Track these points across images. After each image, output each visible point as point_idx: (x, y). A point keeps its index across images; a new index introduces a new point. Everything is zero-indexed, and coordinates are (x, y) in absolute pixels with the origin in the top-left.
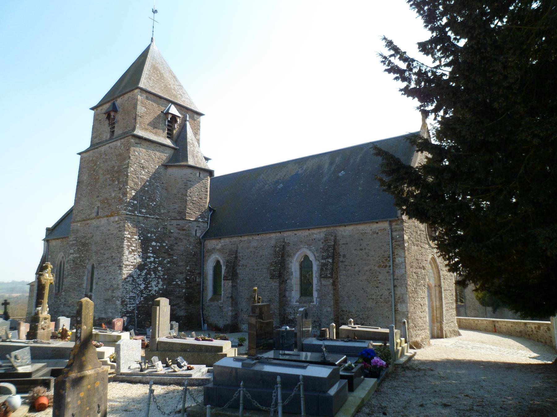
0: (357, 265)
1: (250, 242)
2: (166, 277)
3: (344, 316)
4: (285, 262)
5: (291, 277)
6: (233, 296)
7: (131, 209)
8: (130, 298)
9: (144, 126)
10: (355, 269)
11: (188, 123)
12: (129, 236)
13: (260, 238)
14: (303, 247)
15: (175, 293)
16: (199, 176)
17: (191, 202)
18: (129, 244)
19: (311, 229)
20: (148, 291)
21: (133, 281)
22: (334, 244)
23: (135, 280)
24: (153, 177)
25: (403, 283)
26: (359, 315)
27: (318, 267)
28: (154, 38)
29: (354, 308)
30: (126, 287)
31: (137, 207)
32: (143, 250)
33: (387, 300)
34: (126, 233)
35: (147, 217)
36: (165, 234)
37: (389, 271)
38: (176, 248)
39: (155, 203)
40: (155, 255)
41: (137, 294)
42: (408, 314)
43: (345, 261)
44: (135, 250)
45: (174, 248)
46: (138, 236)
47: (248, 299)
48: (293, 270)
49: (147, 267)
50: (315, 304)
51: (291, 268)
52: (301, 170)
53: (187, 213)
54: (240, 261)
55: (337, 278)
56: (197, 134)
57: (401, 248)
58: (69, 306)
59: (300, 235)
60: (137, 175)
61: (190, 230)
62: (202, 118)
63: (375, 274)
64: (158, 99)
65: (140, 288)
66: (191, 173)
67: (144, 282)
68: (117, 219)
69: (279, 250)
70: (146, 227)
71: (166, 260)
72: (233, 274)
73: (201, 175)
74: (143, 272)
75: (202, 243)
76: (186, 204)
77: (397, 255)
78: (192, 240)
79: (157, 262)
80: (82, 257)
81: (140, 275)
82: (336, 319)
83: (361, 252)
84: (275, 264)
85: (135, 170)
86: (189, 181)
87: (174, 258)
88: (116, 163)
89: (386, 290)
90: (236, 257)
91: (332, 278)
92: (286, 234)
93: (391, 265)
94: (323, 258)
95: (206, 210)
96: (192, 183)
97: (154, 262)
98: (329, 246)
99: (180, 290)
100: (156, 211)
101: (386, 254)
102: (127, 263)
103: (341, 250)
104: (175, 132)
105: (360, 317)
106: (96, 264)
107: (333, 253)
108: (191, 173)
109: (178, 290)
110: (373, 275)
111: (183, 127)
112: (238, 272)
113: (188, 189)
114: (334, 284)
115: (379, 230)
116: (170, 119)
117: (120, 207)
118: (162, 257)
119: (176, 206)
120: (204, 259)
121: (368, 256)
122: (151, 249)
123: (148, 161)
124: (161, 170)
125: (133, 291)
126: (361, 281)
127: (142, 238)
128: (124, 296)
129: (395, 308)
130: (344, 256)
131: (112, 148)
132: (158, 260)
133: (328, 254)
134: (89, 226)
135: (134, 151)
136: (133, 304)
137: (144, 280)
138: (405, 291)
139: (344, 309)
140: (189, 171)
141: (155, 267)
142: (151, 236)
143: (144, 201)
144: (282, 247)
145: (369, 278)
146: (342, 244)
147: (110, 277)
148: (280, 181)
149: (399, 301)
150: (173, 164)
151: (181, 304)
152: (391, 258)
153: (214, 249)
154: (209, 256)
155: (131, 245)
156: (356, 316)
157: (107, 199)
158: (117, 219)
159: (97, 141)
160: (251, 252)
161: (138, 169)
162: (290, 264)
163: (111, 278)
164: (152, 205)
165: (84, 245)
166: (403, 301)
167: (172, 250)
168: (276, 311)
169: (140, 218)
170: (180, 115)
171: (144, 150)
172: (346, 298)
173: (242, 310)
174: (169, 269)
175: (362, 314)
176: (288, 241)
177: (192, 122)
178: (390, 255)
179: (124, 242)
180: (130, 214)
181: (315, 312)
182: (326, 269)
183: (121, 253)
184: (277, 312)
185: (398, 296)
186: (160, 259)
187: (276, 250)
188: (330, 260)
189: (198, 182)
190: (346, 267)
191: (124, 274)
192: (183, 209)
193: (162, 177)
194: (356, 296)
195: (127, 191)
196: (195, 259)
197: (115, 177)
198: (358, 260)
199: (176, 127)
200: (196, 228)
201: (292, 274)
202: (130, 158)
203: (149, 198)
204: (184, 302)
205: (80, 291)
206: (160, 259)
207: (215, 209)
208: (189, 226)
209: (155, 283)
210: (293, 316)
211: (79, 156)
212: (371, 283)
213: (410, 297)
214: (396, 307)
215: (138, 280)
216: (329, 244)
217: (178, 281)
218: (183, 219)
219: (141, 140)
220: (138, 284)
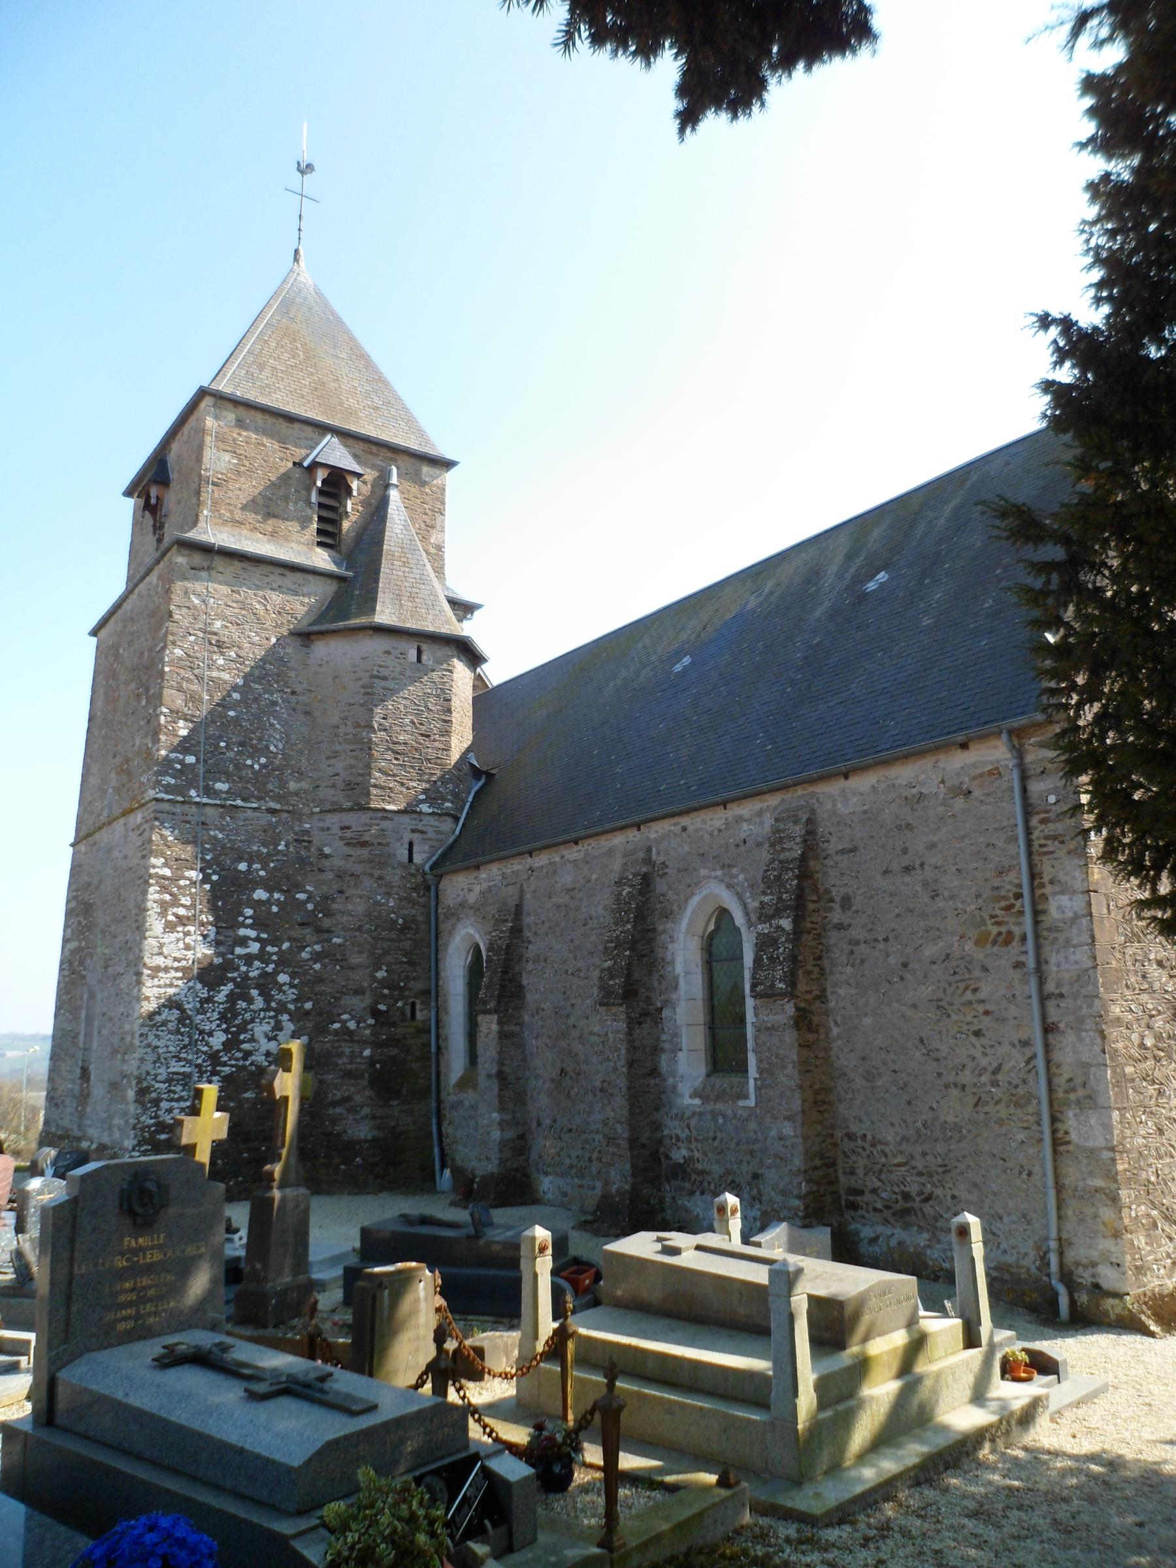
0: (896, 937)
2: (308, 1005)
3: (854, 1158)
4: (651, 940)
5: (674, 996)
6: (507, 1069)
7: (173, 781)
8: (169, 1081)
9: (231, 512)
10: (888, 955)
11: (394, 494)
12: (167, 872)
13: (582, 854)
14: (709, 877)
15: (340, 1062)
16: (419, 660)
17: (389, 749)
18: (167, 897)
20: (239, 1055)
21: (181, 1021)
22: (803, 855)
23: (189, 1017)
24: (257, 673)
25: (1084, 1011)
26: (912, 1157)
28: (301, 251)
29: (892, 1124)
30: (155, 1043)
31: (197, 776)
32: (217, 918)
33: (1021, 1091)
34: (153, 860)
35: (236, 807)
36: (302, 861)
37: (1022, 958)
39: (263, 760)
40: (263, 932)
41: (198, 1066)
42: (1113, 1160)
43: (849, 926)
44: (188, 918)
45: (335, 906)
46: (202, 870)
47: (553, 1080)
48: (679, 969)
49: (235, 975)
51: (673, 963)
53: (375, 786)
54: (530, 942)
55: (822, 997)
56: (433, 527)
57: (1069, 853)
59: (697, 830)
60: (196, 671)
61: (388, 844)
62: (450, 478)
63: (967, 976)
64: (282, 425)
65: (207, 1044)
66: (388, 653)
67: (224, 1026)
69: (629, 893)
70: (230, 840)
71: (308, 949)
73: (424, 657)
74: (219, 992)
75: (433, 888)
76: (371, 756)
77: (1051, 882)
78: (394, 876)
79: (275, 958)
81: (209, 1000)
82: (820, 1173)
83: (908, 879)
84: (615, 948)
85: (189, 656)
86: (378, 677)
87: (335, 940)
89: (1014, 1045)
90: (517, 931)
91: (792, 996)
92: (655, 831)
95: (446, 773)
96: (390, 684)
97: (262, 956)
98: (784, 865)
99: (352, 1052)
100: (270, 786)
101: (1007, 884)
102: (160, 961)
104: (346, 525)
105: (913, 1163)
107: (800, 896)
108: (388, 653)
109: (347, 1051)
110: (957, 977)
111: (377, 508)
112: (525, 982)
113: (376, 706)
115: (975, 778)
116: (324, 482)
118: (289, 939)
119: (339, 765)
120: (440, 942)
121: (935, 896)
122: (249, 912)
123: (238, 624)
124: (289, 650)
125: (183, 1055)
126: (915, 1006)
127: (215, 878)
128: (148, 1073)
129: (1054, 1132)
130: (846, 903)
132: (276, 949)
133: (780, 899)
135: (186, 593)
136: (180, 1099)
137: (223, 1018)
138: (1097, 1048)
139: (854, 1128)
140: (375, 646)
141: (264, 974)
142: (249, 871)
143: (224, 754)
144: (638, 880)
146: (837, 853)
148: (686, 646)
149: (1072, 1096)
150: (334, 626)
151: (358, 1099)
153: (461, 905)
154: (450, 933)
155: (175, 903)
156: (899, 1159)
161: (201, 653)
162: (670, 946)
164: (252, 766)
166: (1090, 1097)
167: (328, 914)
169: (209, 811)
170: (357, 468)
171: (225, 590)
172: (859, 1082)
173: (539, 1124)
175: (924, 1154)
176: (661, 859)
177: (414, 490)
178: (1020, 886)
179: (147, 892)
180: (169, 801)
181: (754, 1137)
182: (771, 959)
183: (140, 928)
185: (1066, 1076)
186: (286, 946)
187: (620, 894)
188: (786, 923)
189: (414, 680)
191: (147, 998)
192: (361, 775)
193: (292, 674)
194: (895, 1072)
195: (159, 724)
196: (407, 945)
198: (898, 916)
199: (349, 509)
200: (407, 837)
201: (676, 987)
202: (171, 616)
203: (241, 744)
204: (368, 1093)
206: (286, 946)
207: (493, 772)
208: (383, 830)
209: (266, 1028)
210: (684, 1152)
212: (954, 1017)
213: (1122, 1080)
214: (1059, 1125)
216: (786, 855)
218: (363, 808)
220: (202, 1032)
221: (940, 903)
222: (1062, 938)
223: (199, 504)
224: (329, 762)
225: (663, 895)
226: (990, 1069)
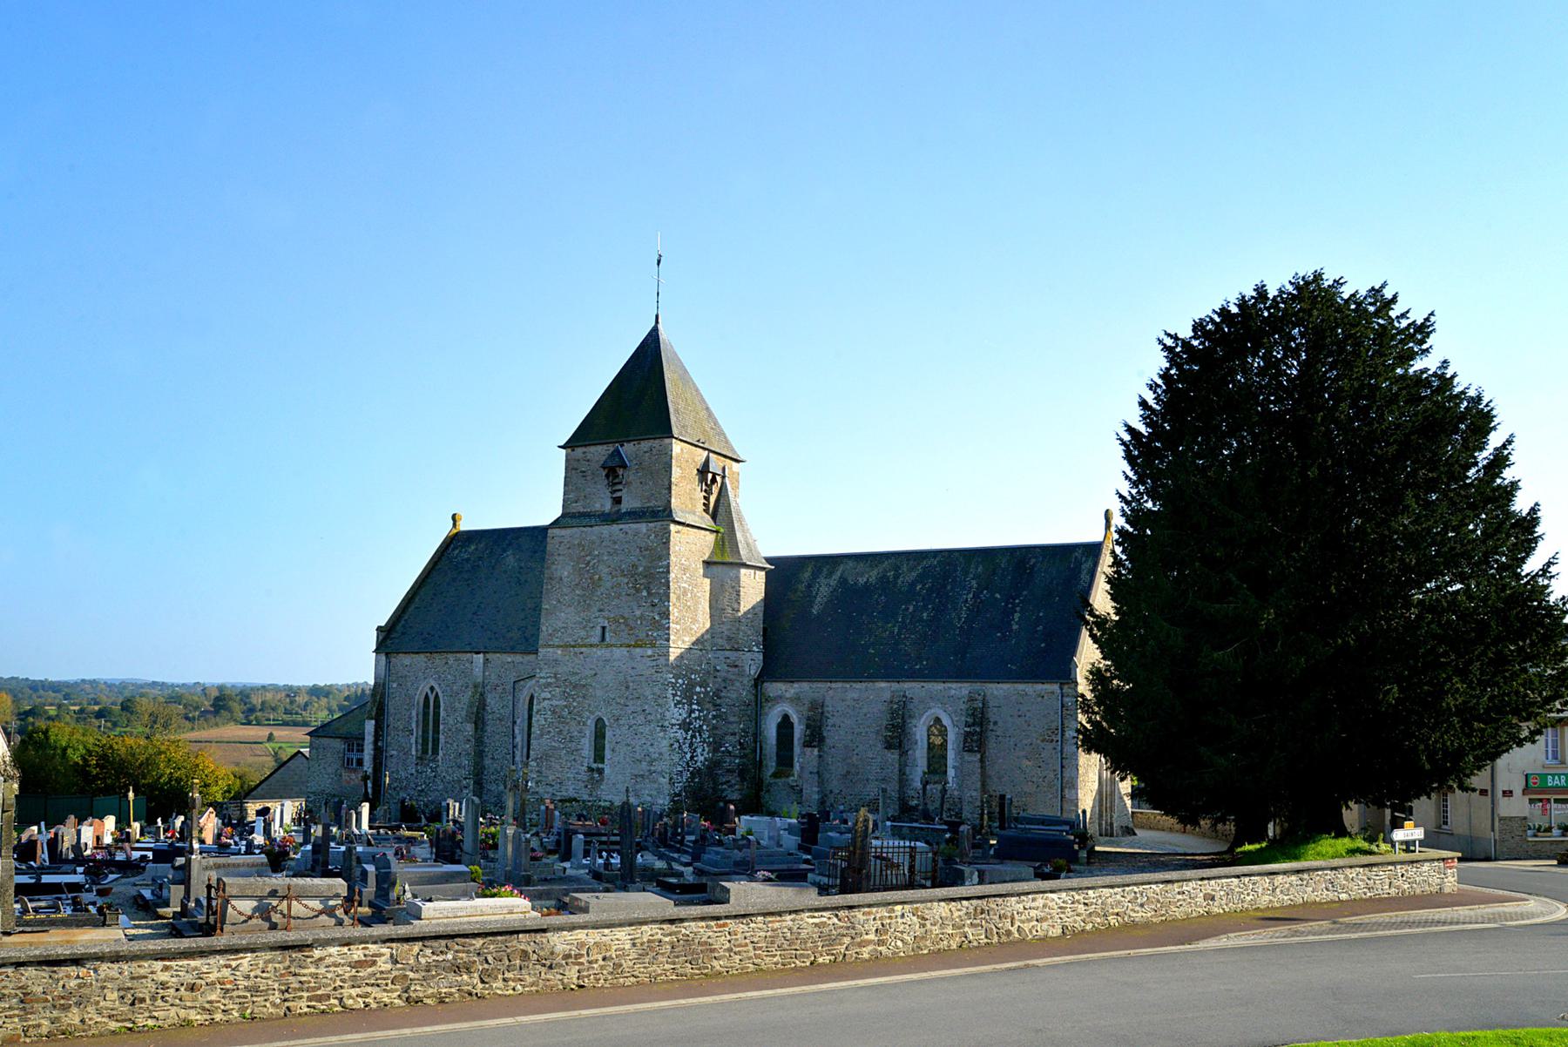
1: (846, 691)
5: (915, 747)
45: (723, 694)
48: (918, 737)
55: (985, 753)
68: (650, 652)
72: (815, 736)
80: (574, 707)
81: (686, 738)
88: (639, 560)
92: (906, 685)
94: (967, 725)
98: (975, 709)
101: (1054, 725)
102: (674, 721)
103: (992, 715)
106: (609, 719)
109: (728, 760)
112: (825, 734)
114: (982, 761)
117: (655, 634)
121: (1029, 725)
130: (995, 723)
134: (584, 658)
136: (680, 782)
137: (690, 747)
151: (733, 782)
152: (1060, 730)
157: (623, 618)
158: (650, 652)
159: (578, 507)
160: (848, 706)
167: (719, 698)
168: (893, 794)
172: (995, 780)
174: (715, 728)
176: (910, 696)
184: (895, 795)
197: (641, 585)
201: (916, 743)
204: (738, 779)
223: (670, 497)
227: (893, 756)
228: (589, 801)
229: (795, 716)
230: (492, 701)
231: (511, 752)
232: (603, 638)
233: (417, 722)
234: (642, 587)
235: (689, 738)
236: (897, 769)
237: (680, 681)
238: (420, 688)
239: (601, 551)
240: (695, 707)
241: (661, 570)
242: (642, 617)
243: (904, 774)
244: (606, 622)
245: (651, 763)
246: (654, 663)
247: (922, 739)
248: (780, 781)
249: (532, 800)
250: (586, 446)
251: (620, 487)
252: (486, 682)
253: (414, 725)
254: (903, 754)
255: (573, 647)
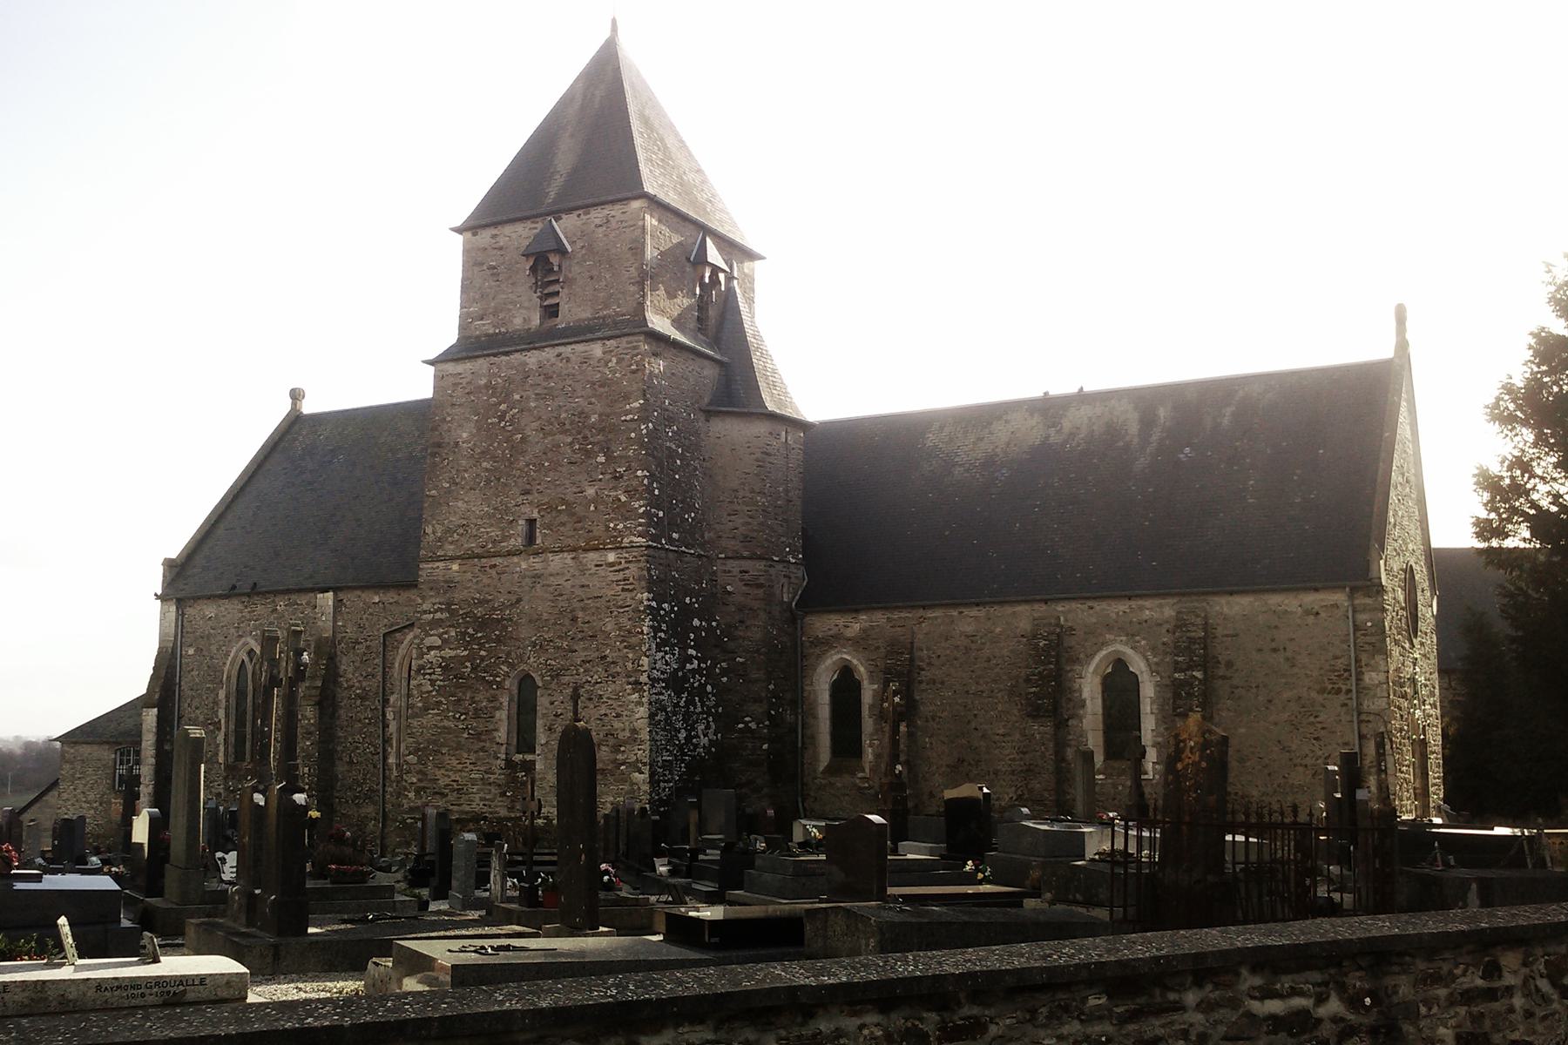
0: (1264, 686)
15: (744, 753)
19: (1137, 596)
27: (1158, 689)
29: (1257, 786)
38: (741, 634)
45: (738, 633)
48: (1086, 694)
50: (1151, 777)
51: (1080, 690)
52: (1058, 432)
58: (444, 795)
63: (1311, 709)
68: (611, 557)
80: (482, 659)
81: (677, 705)
88: (590, 403)
89: (1338, 744)
93: (1354, 688)
97: (698, 671)
98: (1192, 641)
101: (1340, 664)
106: (542, 676)
109: (750, 745)
115: (1322, 607)
117: (621, 526)
126: (1276, 724)
130: (1229, 664)
131: (568, 360)
144: (1054, 637)
145: (1296, 717)
146: (1223, 636)
147: (603, 712)
154: (819, 657)
157: (563, 502)
158: (611, 557)
159: (486, 327)
163: (606, 715)
165: (483, 624)
169: (671, 555)
178: (1349, 665)
190: (1236, 691)
198: (1266, 674)
201: (1083, 705)
205: (483, 749)
211: (431, 369)
215: (674, 718)
217: (750, 722)
219: (663, 345)
221: (1296, 670)
222: (1372, 693)
224: (729, 518)
225: (1071, 648)
226: (1324, 756)
227: (1041, 730)
228: (509, 819)
229: (862, 669)
230: (346, 665)
231: (380, 750)
232: (530, 538)
233: (227, 708)
234: (596, 449)
235: (682, 704)
236: (1051, 752)
237: (665, 606)
238: (232, 655)
239: (524, 394)
240: (692, 652)
241: (628, 418)
242: (597, 500)
243: (1064, 760)
244: (536, 511)
245: (616, 749)
246: (621, 576)
247: (1092, 699)
248: (839, 782)
249: (409, 821)
250: (495, 355)
251: (556, 288)
252: (339, 636)
253: (221, 713)
254: (1061, 725)
255: (479, 557)
